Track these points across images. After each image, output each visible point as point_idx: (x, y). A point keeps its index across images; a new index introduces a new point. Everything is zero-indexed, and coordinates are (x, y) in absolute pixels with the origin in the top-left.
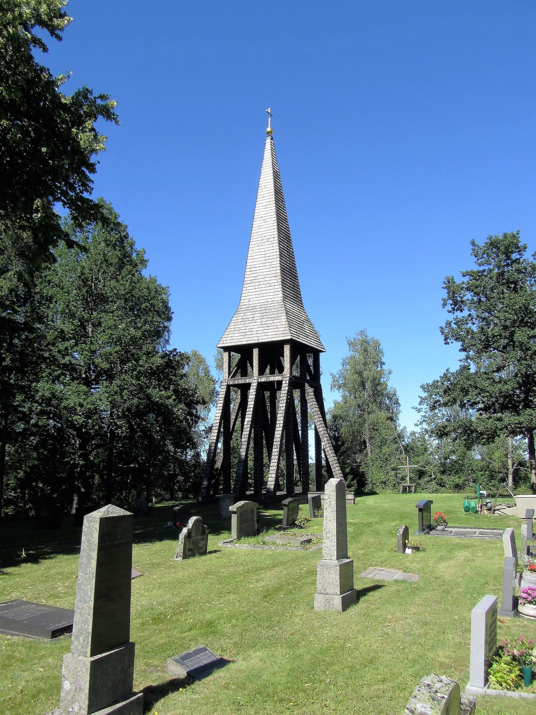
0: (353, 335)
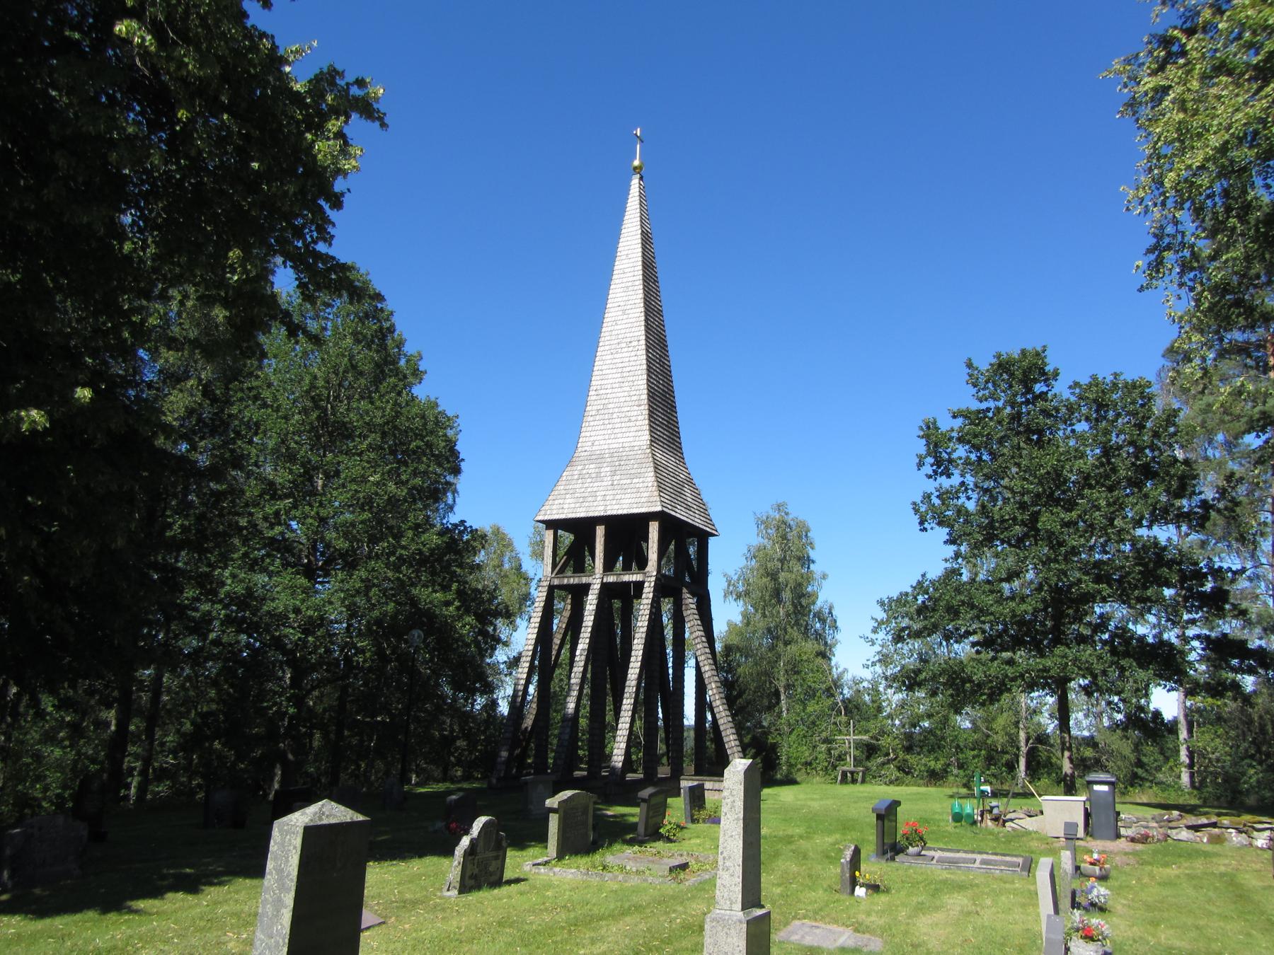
0: (765, 508)
